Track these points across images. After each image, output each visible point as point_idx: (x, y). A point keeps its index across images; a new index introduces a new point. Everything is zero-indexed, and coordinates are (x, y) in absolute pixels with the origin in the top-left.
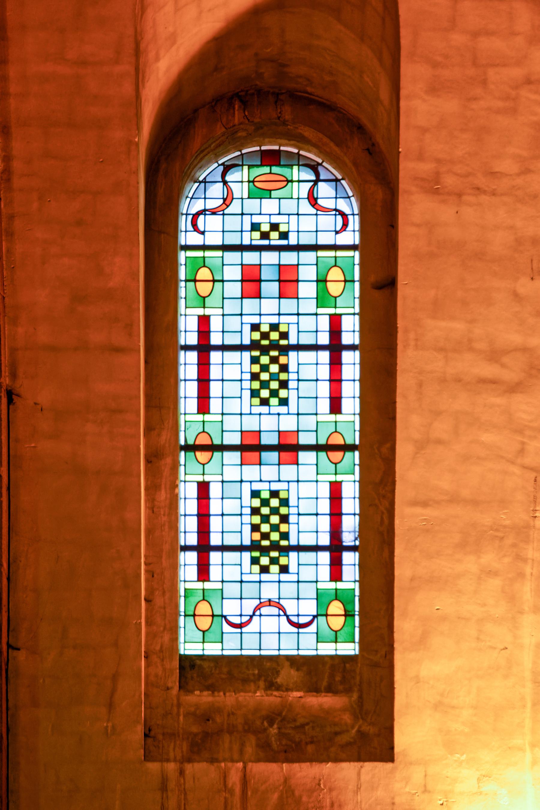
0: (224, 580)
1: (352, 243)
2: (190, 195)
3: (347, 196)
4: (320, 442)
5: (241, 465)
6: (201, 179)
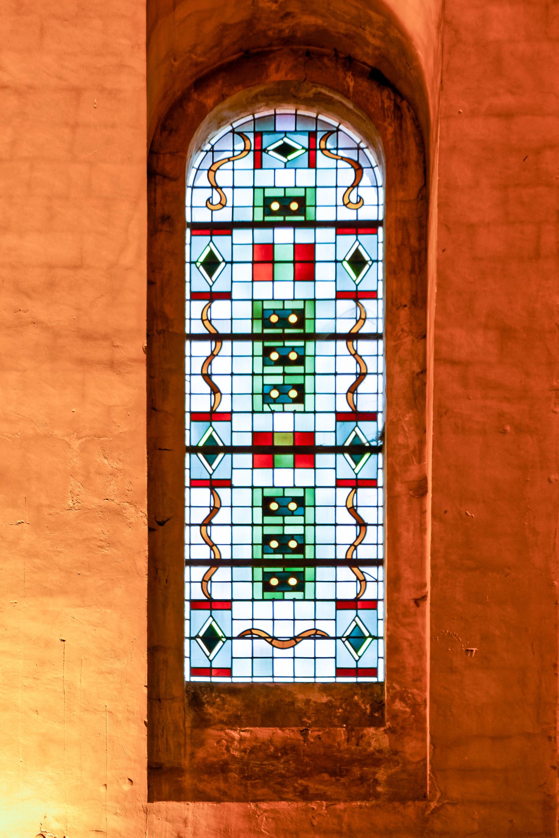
0: (236, 185)
2: (196, 166)
4: (339, 557)
5: (253, 281)
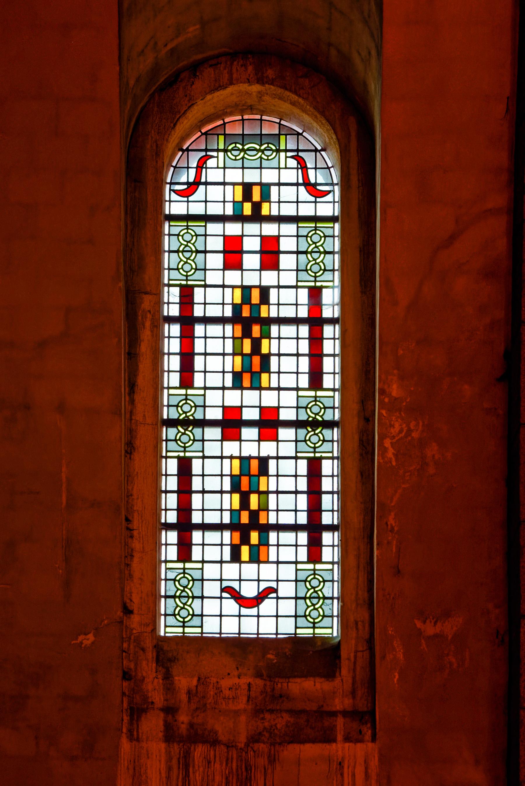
1: (331, 214)
3: (326, 167)
6: (185, 148)
